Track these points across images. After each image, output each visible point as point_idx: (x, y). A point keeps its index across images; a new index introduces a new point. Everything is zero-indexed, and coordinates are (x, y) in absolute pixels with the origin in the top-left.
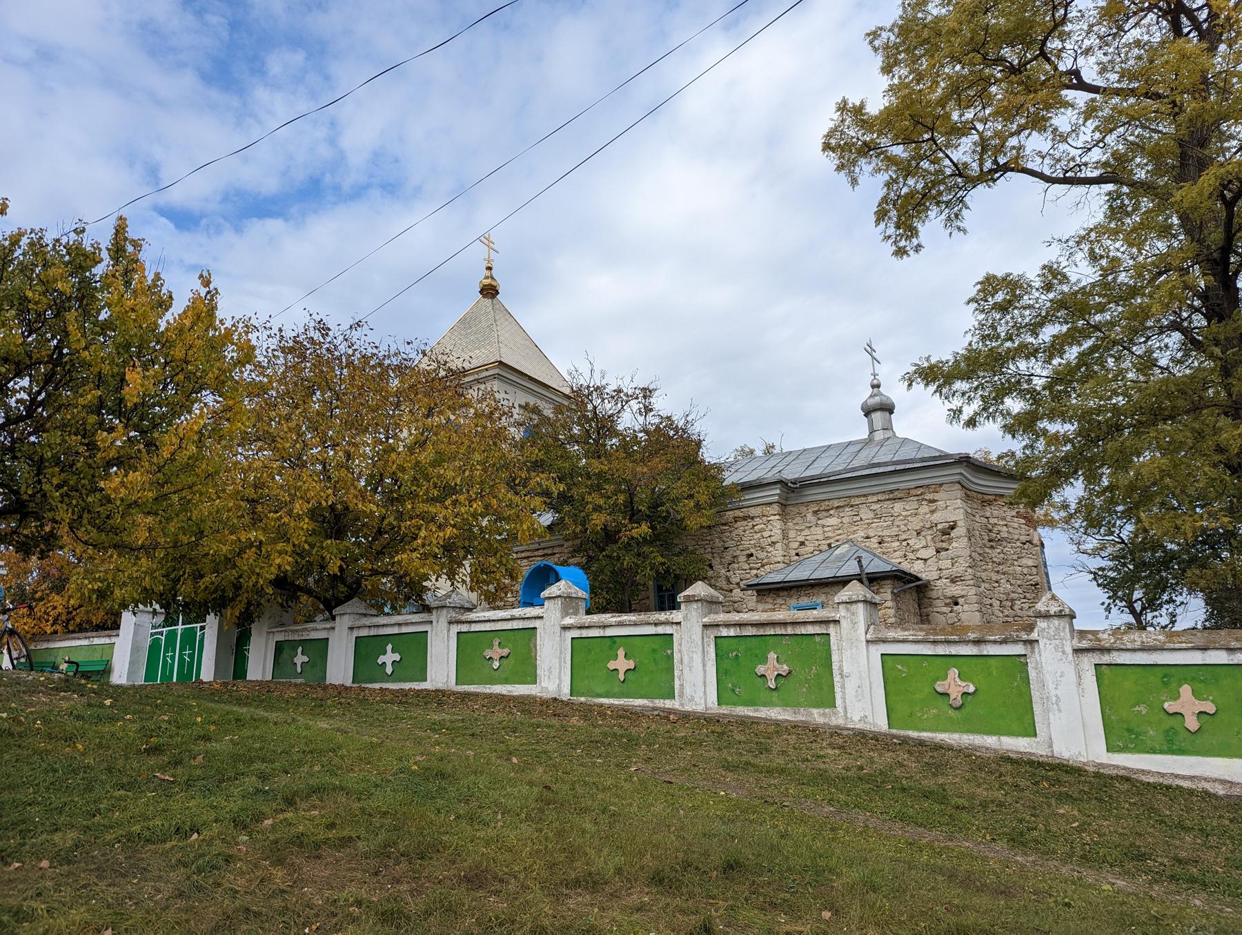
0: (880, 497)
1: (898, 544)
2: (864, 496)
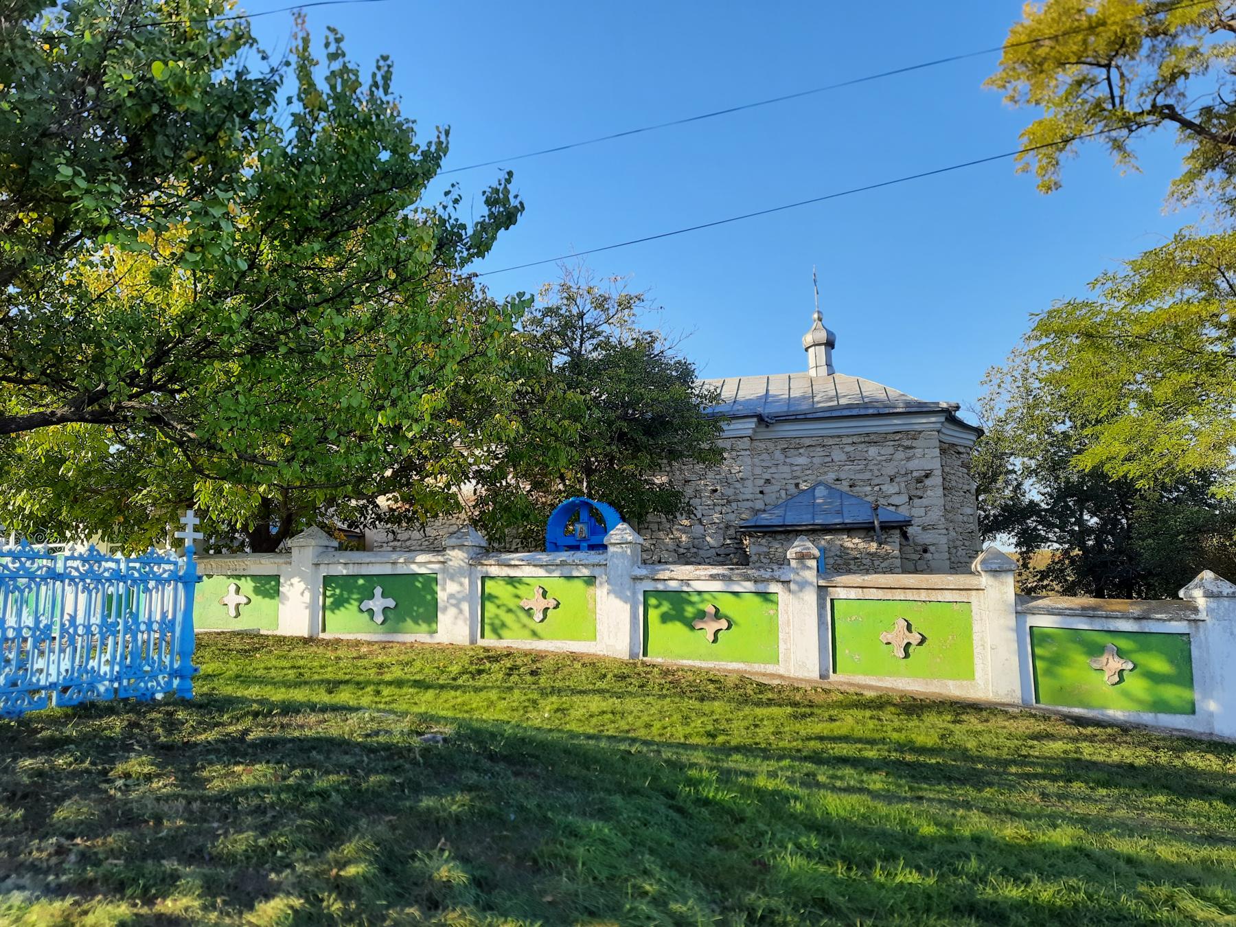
0: (855, 439)
1: (869, 488)
2: (839, 436)
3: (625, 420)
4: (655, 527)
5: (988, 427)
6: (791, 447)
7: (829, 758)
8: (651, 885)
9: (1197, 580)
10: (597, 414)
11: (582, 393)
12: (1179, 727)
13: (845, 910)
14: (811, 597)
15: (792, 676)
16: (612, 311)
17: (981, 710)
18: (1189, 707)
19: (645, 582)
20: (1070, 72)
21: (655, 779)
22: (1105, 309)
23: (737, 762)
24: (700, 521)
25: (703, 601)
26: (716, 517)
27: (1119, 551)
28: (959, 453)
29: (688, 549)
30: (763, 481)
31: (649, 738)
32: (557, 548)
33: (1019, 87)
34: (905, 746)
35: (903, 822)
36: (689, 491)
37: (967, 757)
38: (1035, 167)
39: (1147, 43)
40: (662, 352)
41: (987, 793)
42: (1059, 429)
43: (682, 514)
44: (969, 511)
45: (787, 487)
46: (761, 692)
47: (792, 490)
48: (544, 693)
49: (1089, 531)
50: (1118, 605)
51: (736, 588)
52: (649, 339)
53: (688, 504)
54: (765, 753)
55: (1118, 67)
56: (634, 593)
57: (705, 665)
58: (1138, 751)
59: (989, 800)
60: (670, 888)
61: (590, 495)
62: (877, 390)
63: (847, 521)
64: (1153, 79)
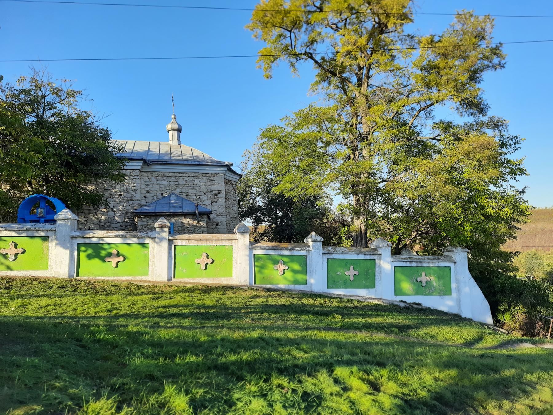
0: (189, 175)
1: (195, 197)
2: (182, 173)
3: (70, 155)
4: (87, 212)
5: (244, 174)
6: (160, 176)
7: (167, 315)
8: (59, 383)
9: (310, 235)
10: (52, 151)
11: (43, 138)
12: (302, 289)
13: (160, 378)
14: (165, 245)
15: (154, 281)
16: (63, 97)
17: (234, 289)
18: (305, 282)
19: (78, 239)
20: (277, 30)
21: (73, 333)
22: (286, 130)
23: (122, 321)
24: (112, 210)
25: (110, 248)
26: (121, 208)
27: (288, 225)
28: (232, 184)
29: (105, 223)
30: (145, 191)
31: (74, 315)
32: (24, 221)
33: (258, 32)
34: (201, 306)
35: (194, 337)
36: (107, 194)
37: (226, 308)
38: (263, 67)
39: (305, 26)
40: (93, 123)
41: (232, 321)
42: (270, 177)
43: (102, 206)
44: (235, 208)
45: (157, 195)
46: (138, 289)
47: (160, 196)
48: (12, 298)
49: (279, 217)
50: (284, 245)
51: (129, 241)
52: (85, 115)
53: (106, 201)
54: (136, 316)
55: (294, 33)
56: (72, 245)
57: (110, 279)
58: (287, 299)
59: (232, 324)
60: (70, 382)
61: (47, 194)
62: (199, 154)
63: (184, 211)
64: (306, 41)
